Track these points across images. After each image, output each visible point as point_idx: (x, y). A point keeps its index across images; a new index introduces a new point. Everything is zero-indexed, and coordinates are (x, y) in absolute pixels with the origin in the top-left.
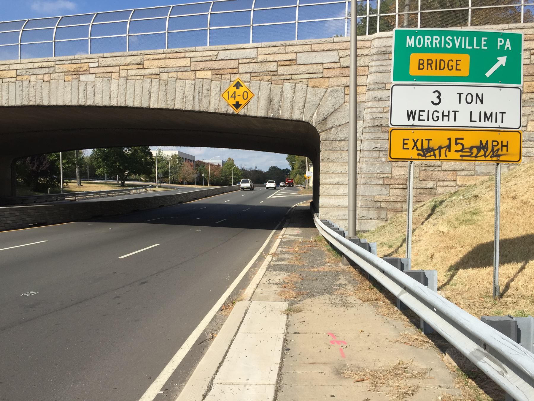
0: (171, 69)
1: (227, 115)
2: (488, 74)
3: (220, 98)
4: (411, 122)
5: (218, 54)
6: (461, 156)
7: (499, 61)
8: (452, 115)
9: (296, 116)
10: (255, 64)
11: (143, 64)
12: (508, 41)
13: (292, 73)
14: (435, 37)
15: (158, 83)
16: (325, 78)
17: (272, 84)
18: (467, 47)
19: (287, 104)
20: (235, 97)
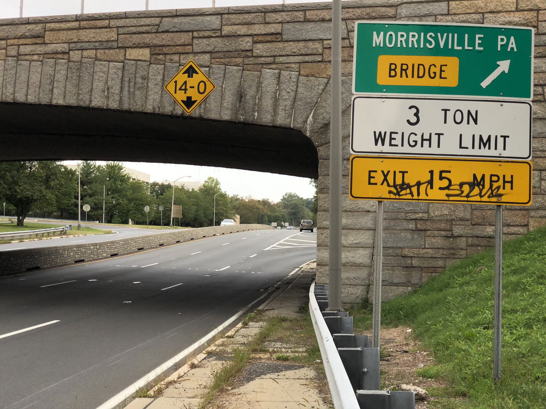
0: (87, 44)
1: (173, 117)
2: (485, 84)
3: (162, 91)
4: (379, 148)
5: (160, 22)
6: (448, 195)
7: (499, 66)
8: (435, 139)
9: (281, 120)
10: (217, 39)
11: (44, 37)
12: (512, 39)
13: (276, 54)
14: (411, 34)
15: (66, 67)
16: (326, 62)
17: (243, 70)
18: (456, 48)
19: (267, 103)
20: (186, 90)
